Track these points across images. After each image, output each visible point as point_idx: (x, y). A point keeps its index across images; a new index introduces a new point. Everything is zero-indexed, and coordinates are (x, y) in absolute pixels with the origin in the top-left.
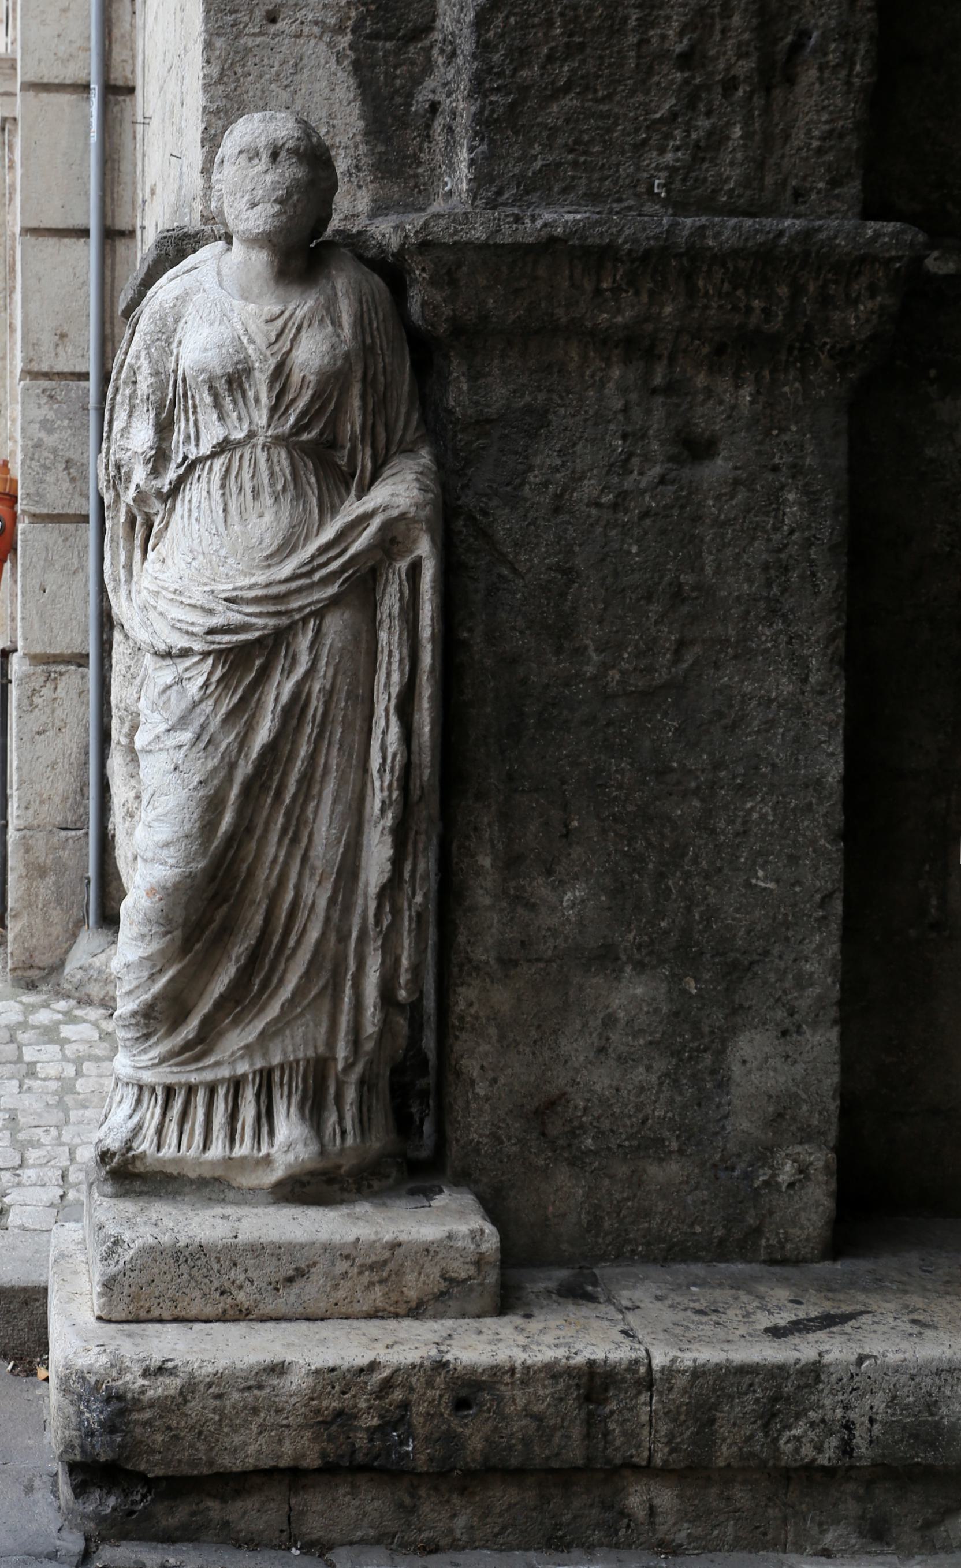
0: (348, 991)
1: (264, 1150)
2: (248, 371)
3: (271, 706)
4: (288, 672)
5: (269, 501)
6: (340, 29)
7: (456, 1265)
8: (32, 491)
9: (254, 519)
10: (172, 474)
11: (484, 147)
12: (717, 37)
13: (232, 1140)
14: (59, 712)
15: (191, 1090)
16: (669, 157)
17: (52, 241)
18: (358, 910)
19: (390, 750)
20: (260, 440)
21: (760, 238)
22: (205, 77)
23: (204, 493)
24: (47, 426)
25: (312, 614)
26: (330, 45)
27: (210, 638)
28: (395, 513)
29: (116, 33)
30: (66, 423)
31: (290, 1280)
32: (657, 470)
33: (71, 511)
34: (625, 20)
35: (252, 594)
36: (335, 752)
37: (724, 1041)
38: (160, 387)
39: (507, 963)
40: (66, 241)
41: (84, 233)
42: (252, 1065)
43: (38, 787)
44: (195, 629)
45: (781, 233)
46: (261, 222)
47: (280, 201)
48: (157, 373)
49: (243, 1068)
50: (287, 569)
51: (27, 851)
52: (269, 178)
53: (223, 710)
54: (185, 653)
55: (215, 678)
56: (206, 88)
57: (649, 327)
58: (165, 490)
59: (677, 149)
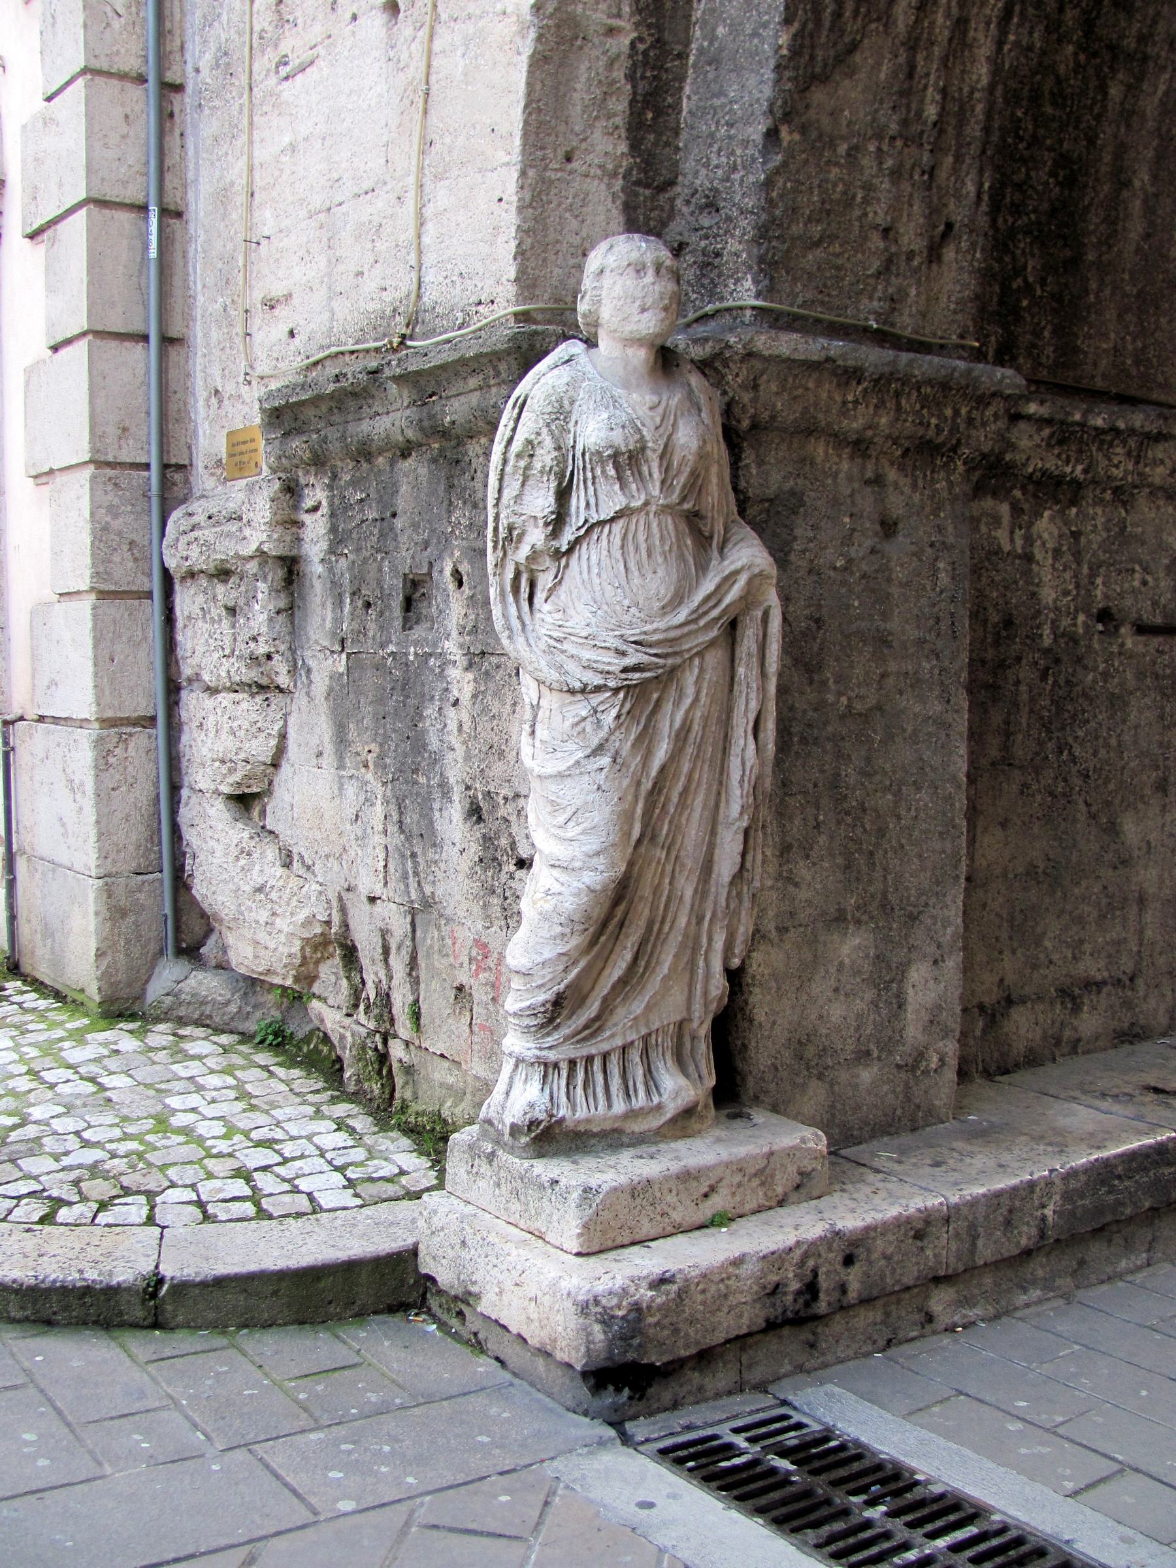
0: (701, 964)
1: (656, 1099)
2: (643, 449)
3: (667, 729)
4: (677, 704)
5: (660, 560)
6: (614, 175)
7: (806, 1162)
8: (101, 569)
9: (649, 576)
10: (568, 535)
11: (767, 282)
12: (905, 219)
13: (628, 1095)
14: (130, 768)
15: (589, 1059)
16: (875, 303)
17: (114, 344)
18: (711, 898)
19: (748, 765)
20: (653, 508)
21: (943, 372)
22: (520, 200)
23: (605, 553)
24: (112, 510)
25: (696, 654)
26: (609, 186)
27: (623, 676)
28: (757, 571)
29: (168, 162)
30: (129, 508)
31: (706, 1196)
32: (868, 543)
33: (134, 588)
34: (854, 197)
35: (656, 637)
36: (706, 767)
37: (903, 972)
38: (561, 460)
39: (782, 930)
40: (127, 344)
41: (145, 338)
42: (638, 1031)
43: (115, 838)
44: (611, 669)
45: (954, 369)
46: (651, 324)
47: (666, 309)
48: (559, 448)
49: (632, 1036)
50: (682, 615)
51: (109, 897)
52: (657, 288)
53: (632, 737)
54: (598, 689)
55: (625, 710)
56: (520, 209)
57: (870, 433)
58: (564, 549)
59: (880, 299)
